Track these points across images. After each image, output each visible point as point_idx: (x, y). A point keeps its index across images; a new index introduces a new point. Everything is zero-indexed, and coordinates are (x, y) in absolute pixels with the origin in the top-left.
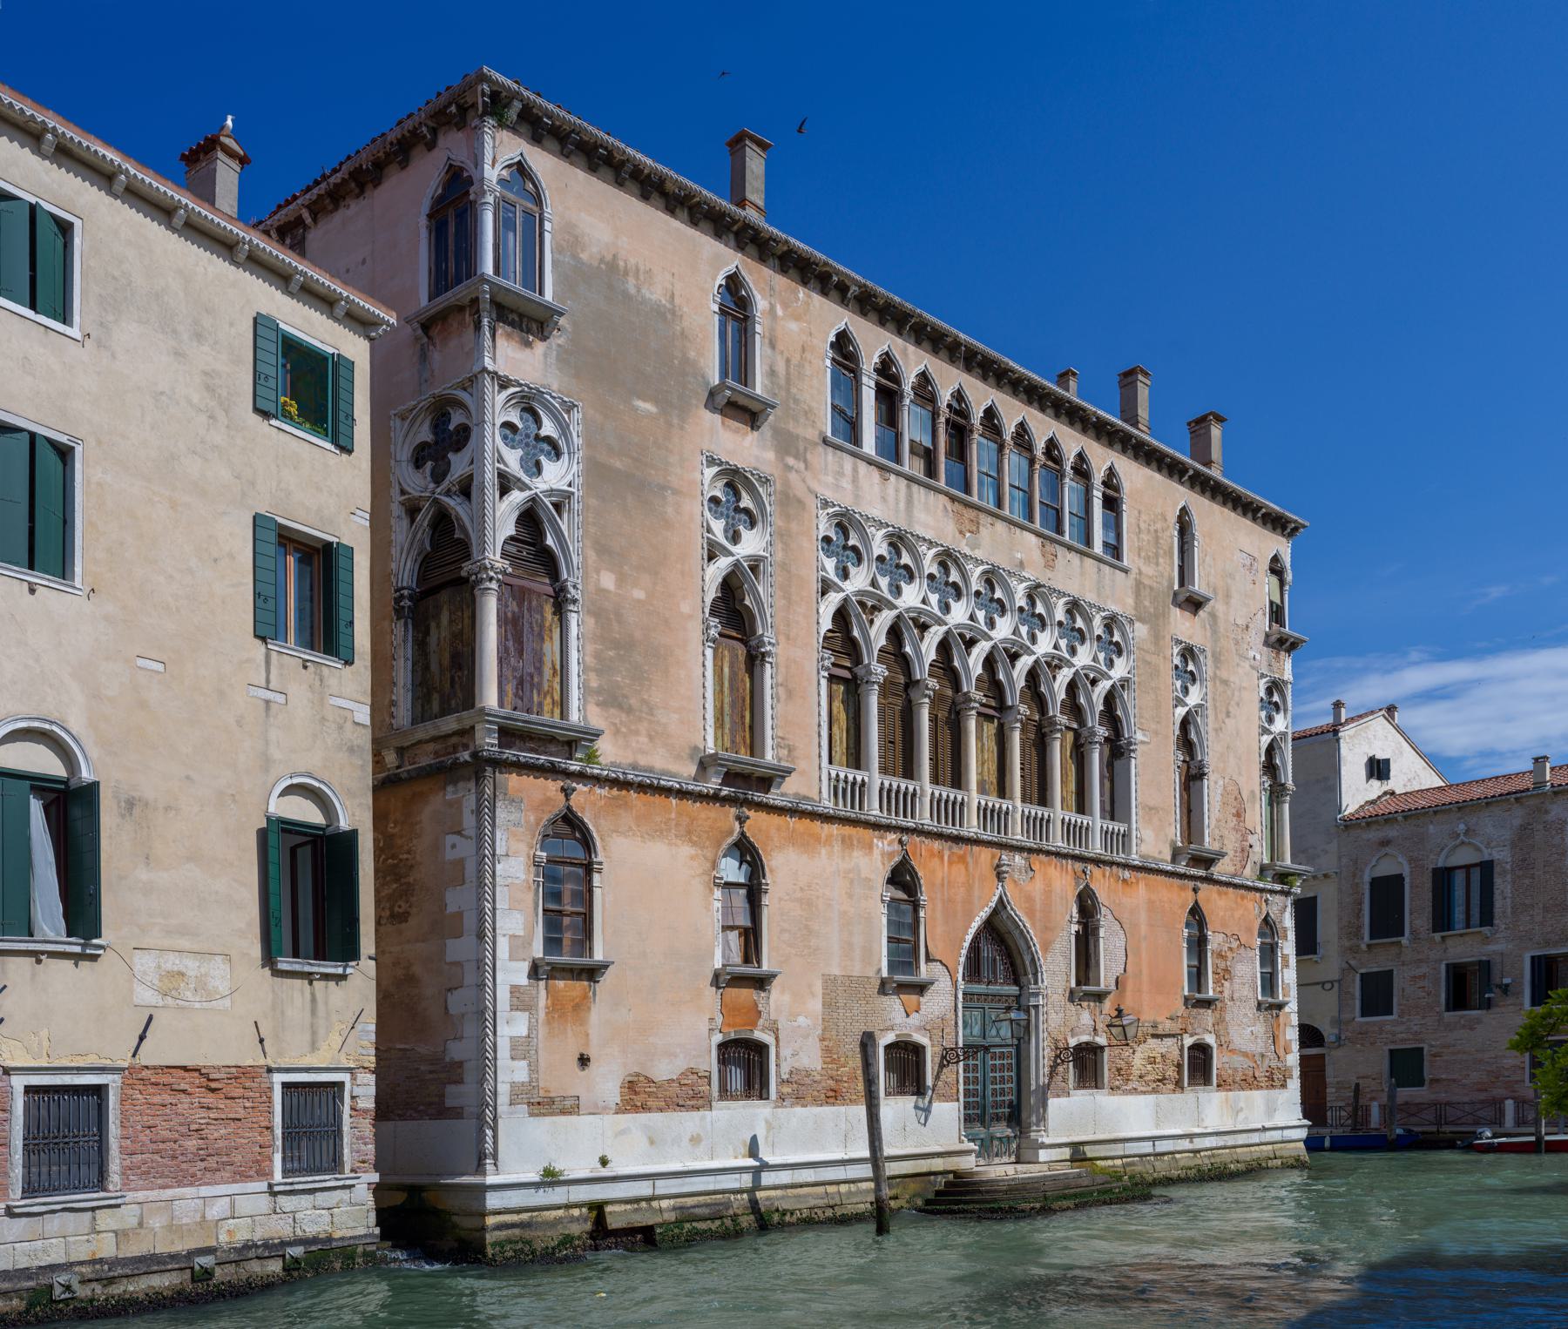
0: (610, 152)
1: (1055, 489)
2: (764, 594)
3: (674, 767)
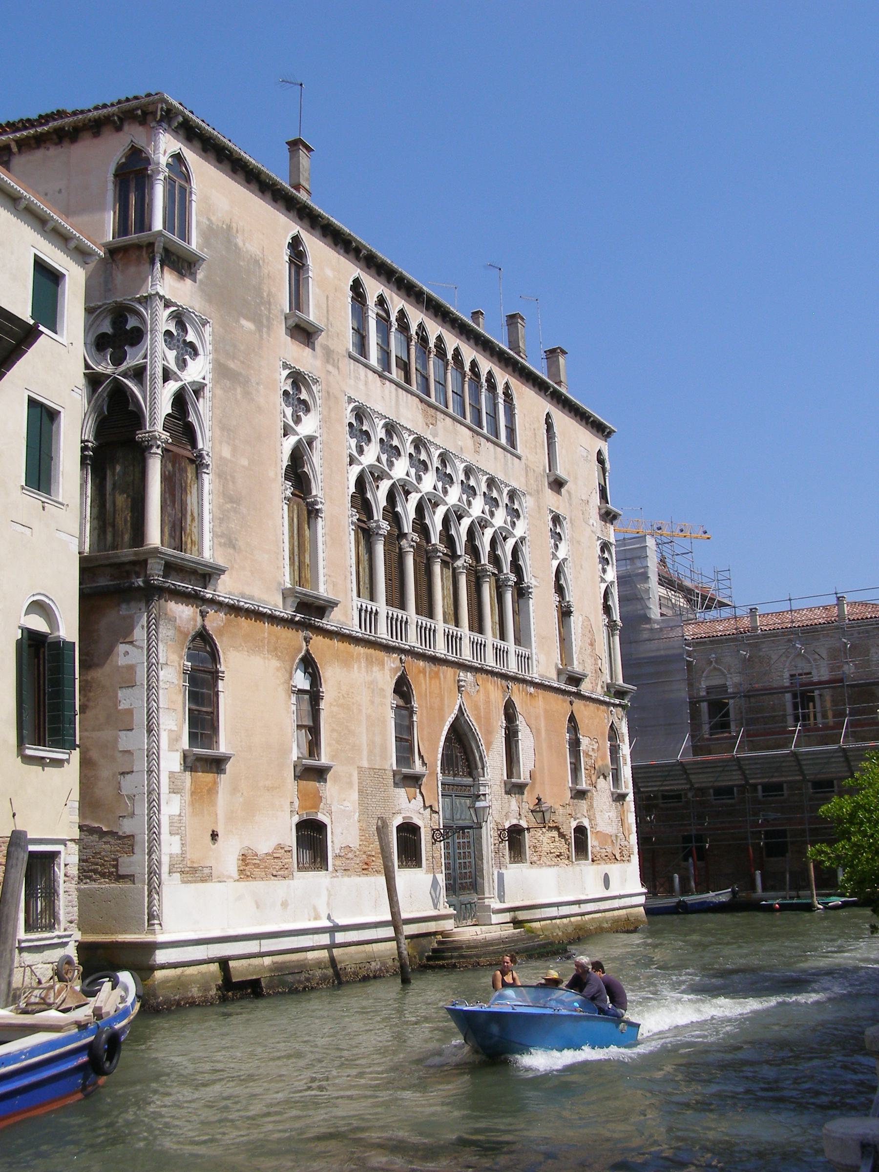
0: (231, 153)
1: (476, 397)
2: (317, 464)
3: (265, 597)
